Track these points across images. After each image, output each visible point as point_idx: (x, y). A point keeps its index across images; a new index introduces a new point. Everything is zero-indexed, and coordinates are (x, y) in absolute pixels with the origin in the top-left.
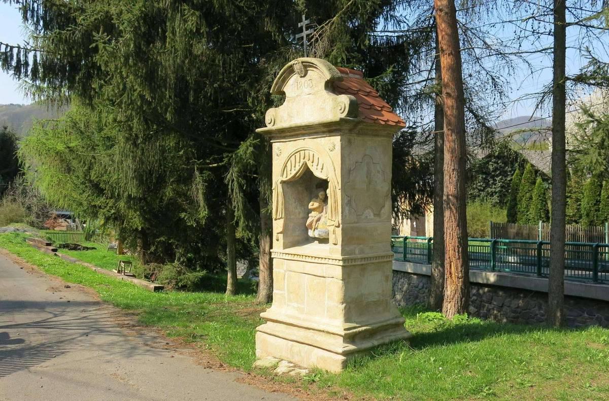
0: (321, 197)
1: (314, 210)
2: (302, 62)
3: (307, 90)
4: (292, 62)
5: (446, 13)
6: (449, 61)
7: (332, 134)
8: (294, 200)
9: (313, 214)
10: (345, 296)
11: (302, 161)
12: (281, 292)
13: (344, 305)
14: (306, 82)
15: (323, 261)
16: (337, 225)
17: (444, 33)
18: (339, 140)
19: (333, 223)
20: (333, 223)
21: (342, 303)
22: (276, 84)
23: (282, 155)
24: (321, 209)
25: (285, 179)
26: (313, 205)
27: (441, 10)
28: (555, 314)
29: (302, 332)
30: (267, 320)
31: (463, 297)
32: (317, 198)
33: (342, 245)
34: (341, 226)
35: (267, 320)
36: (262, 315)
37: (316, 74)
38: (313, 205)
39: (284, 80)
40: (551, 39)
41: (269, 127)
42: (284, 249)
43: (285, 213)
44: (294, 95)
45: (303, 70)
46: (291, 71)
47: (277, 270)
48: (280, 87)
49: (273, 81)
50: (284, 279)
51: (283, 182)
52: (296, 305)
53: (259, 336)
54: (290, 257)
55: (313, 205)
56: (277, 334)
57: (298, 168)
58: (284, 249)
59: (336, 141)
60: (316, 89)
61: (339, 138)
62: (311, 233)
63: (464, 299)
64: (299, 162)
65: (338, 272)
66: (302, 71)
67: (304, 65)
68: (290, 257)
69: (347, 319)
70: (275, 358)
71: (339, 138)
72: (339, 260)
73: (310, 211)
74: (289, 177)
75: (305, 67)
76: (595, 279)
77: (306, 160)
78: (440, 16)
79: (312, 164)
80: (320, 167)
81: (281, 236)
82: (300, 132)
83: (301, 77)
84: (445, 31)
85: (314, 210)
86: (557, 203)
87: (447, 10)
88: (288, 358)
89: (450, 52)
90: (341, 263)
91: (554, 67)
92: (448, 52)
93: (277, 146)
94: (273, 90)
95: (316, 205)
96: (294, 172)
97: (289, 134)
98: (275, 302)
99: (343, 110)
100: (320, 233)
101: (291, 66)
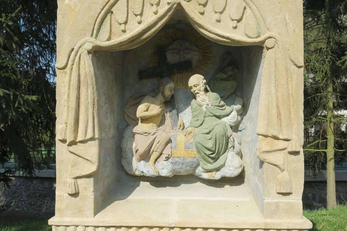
1: (145, 120)
20: (281, 144)
24: (160, 119)
25: (103, 42)
42: (96, 213)
51: (97, 53)
62: (139, 167)
73: (135, 121)
85: (145, 120)
95: (155, 109)
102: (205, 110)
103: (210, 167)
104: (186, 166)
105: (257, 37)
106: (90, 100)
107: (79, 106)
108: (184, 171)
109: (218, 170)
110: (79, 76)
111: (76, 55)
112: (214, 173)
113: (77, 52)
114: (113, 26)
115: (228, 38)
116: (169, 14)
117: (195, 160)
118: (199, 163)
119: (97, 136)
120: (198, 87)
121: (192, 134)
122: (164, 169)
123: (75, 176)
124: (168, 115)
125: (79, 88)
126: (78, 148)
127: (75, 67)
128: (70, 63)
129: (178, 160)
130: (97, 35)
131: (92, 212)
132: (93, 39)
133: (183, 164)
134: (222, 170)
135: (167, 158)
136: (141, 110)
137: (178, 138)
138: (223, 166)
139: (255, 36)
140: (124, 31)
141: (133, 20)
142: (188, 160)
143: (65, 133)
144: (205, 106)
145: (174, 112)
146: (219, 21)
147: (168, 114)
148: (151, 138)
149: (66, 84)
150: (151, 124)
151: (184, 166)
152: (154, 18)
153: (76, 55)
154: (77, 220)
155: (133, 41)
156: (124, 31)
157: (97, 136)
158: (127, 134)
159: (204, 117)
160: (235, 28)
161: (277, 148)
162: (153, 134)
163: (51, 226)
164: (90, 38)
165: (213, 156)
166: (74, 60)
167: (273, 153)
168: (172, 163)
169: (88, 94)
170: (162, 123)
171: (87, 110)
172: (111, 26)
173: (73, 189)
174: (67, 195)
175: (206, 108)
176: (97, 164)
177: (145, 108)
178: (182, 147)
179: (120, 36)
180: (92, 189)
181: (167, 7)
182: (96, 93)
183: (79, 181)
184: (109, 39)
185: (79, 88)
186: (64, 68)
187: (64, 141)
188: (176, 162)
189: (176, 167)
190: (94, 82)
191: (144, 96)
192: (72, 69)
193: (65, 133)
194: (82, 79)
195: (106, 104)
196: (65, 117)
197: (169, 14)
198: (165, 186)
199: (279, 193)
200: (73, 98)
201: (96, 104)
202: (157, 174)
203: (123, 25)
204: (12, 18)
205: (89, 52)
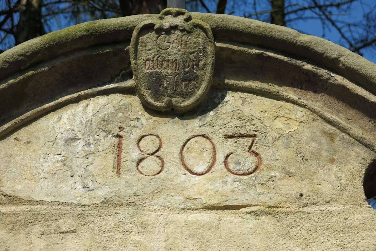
2: (220, 33)
37: (299, 113)
44: (72, 191)
60: (291, 187)
101: (122, 36)
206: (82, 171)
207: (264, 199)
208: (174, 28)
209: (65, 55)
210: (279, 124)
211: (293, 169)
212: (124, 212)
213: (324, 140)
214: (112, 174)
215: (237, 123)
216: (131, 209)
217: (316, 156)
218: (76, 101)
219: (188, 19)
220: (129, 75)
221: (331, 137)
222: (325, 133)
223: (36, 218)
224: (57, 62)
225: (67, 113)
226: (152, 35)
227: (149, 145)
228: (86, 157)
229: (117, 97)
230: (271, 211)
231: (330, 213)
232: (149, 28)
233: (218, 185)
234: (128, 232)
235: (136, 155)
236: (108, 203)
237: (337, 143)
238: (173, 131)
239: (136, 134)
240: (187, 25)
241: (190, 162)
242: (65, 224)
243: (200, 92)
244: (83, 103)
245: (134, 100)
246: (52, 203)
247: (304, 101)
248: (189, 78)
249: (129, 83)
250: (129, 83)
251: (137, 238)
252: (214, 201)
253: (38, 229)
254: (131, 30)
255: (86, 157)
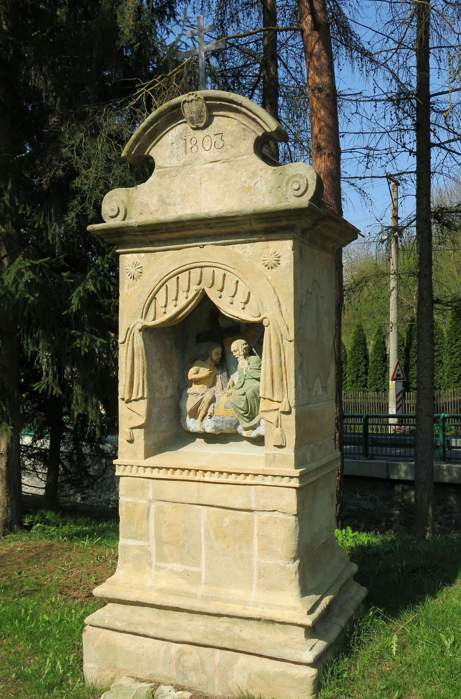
0: (215, 357)
1: (198, 381)
2: (206, 99)
3: (210, 155)
4: (182, 98)
5: (328, 95)
6: (329, 164)
7: (274, 236)
8: (158, 365)
9: (195, 388)
10: (299, 545)
11: (194, 288)
12: (140, 543)
13: (298, 562)
14: (207, 139)
15: (249, 480)
16: (287, 410)
17: (322, 124)
18: (290, 248)
19: (275, 405)
20: (275, 405)
21: (295, 559)
22: (136, 141)
23: (145, 276)
24: (211, 380)
25: (150, 322)
26: (197, 373)
27: (320, 90)
28: (427, 511)
29: (200, 621)
30: (104, 602)
31: (338, 503)
32: (205, 360)
33: (297, 448)
34: (294, 410)
35: (104, 602)
36: (98, 591)
37: (235, 122)
38: (197, 372)
39: (154, 134)
40: (413, 160)
41: (110, 223)
42: (146, 457)
43: (149, 390)
44: (174, 162)
45: (205, 114)
46: (174, 115)
47: (129, 499)
48: (143, 147)
49: (130, 138)
50: (148, 517)
51: (145, 330)
52: (178, 567)
53: (89, 635)
54: (162, 474)
55: (197, 373)
56: (140, 630)
57: (182, 302)
58: (146, 457)
59: (283, 250)
60: (233, 151)
61: (288, 245)
62: (192, 425)
63: (339, 505)
64: (188, 291)
65: (289, 500)
66: (201, 116)
67: (207, 105)
68: (162, 474)
69: (305, 591)
70: (142, 681)
71: (288, 245)
72: (291, 477)
73: (189, 383)
74: (161, 319)
75: (210, 108)
76: (366, 455)
77: (205, 286)
78: (318, 98)
79: (219, 294)
80: (241, 297)
81: (139, 435)
82: (191, 233)
83: (197, 129)
84: (324, 121)
85: (198, 381)
86: (426, 367)
87: (328, 91)
88: (170, 679)
89: (330, 152)
90: (295, 483)
91: (417, 196)
92: (327, 151)
93: (129, 261)
94: (129, 152)
95: (204, 372)
96: (172, 311)
97: (167, 235)
98: (125, 562)
99: (302, 189)
100: (218, 425)
101: (178, 106)
102: (245, 373)
103: (247, 425)
104: (226, 424)
105: (258, 317)
106: (141, 368)
107: (133, 372)
108: (226, 428)
109: (254, 428)
110: (133, 349)
111: (131, 333)
112: (250, 431)
113: (132, 331)
114: (157, 309)
115: (237, 317)
116: (197, 298)
117: (234, 419)
118: (239, 422)
119: (146, 396)
120: (238, 352)
121: (232, 395)
122: (209, 426)
123: (131, 427)
124: (219, 377)
125: (133, 358)
126: (133, 405)
127: (130, 342)
128: (127, 339)
129: (218, 418)
130: (145, 317)
131: (142, 455)
132: (142, 320)
133: (223, 422)
134: (258, 428)
135: (211, 417)
136: (192, 374)
137: (222, 399)
138: (258, 424)
139: (257, 316)
140: (165, 313)
141: (171, 304)
142: (227, 418)
143: (124, 393)
144: (245, 369)
145: (225, 374)
146: (232, 303)
147: (219, 375)
148: (199, 398)
149: (125, 355)
150: (202, 385)
151: (224, 424)
152: (185, 302)
153: (131, 333)
154: (131, 462)
155: (171, 320)
156: (165, 313)
157: (146, 396)
158: (183, 394)
159: (244, 379)
160: (244, 309)
161: (271, 409)
162: (202, 395)
163: (115, 465)
164: (140, 320)
165: (246, 415)
166: (129, 337)
167: (269, 413)
168: (215, 421)
169: (140, 363)
170: (214, 384)
171: (139, 375)
172: (155, 309)
173: (129, 436)
174: (126, 441)
175: (246, 371)
176: (145, 418)
177: (195, 372)
178: (222, 406)
179: (162, 316)
180: (143, 437)
181: (195, 293)
182: (145, 361)
183: (135, 431)
184: (154, 319)
185: (133, 358)
186: (123, 343)
187: (123, 399)
188: (217, 420)
189: (218, 425)
190: (144, 354)
191: (197, 359)
192: (128, 344)
193: (124, 393)
194: (135, 351)
195: (160, 368)
196: (124, 381)
197: (197, 298)
198: (214, 443)
199: (275, 446)
200: (129, 366)
201: (145, 370)
202: (202, 430)
203: (174, 301)
204: (108, 259)
205: (140, 331)
206: (176, 155)
207: (225, 157)
208: (193, 100)
209: (164, 115)
210: (229, 128)
211: (233, 145)
212: (188, 167)
213: (242, 132)
214: (184, 154)
215: (217, 129)
216: (190, 166)
217: (240, 138)
218: (172, 128)
219: (196, 96)
220: (184, 118)
221: (244, 130)
222: (243, 129)
223: (166, 172)
224: (163, 118)
225: (170, 133)
226: (187, 103)
227: (193, 141)
228: (177, 149)
229: (183, 124)
230: (227, 161)
231: (243, 159)
232: (185, 101)
233: (213, 154)
234: (190, 174)
235: (190, 146)
236: (184, 165)
237: (246, 132)
238: (200, 134)
239: (190, 139)
240: (196, 98)
241: (205, 146)
242: (174, 174)
243: (205, 120)
244: (174, 129)
245: (186, 125)
246: (170, 167)
247: (236, 118)
248: (201, 116)
249: (185, 120)
250: (185, 120)
251: (192, 176)
252: (212, 160)
253: (167, 176)
254: (180, 103)
255: (177, 149)
